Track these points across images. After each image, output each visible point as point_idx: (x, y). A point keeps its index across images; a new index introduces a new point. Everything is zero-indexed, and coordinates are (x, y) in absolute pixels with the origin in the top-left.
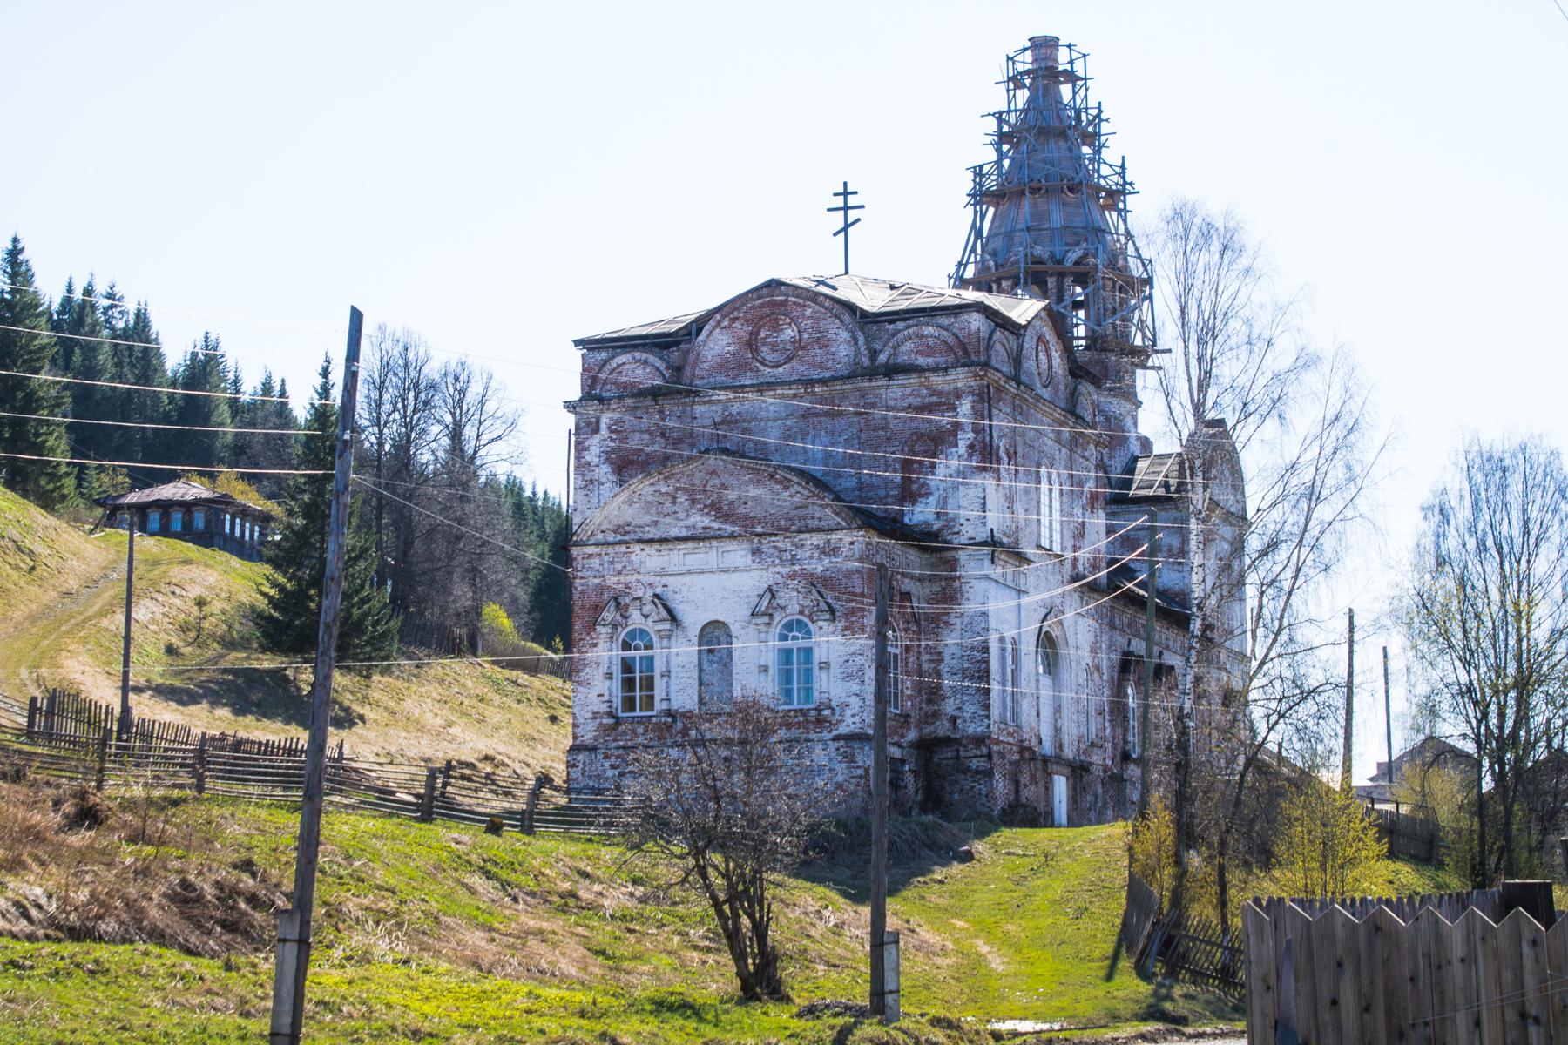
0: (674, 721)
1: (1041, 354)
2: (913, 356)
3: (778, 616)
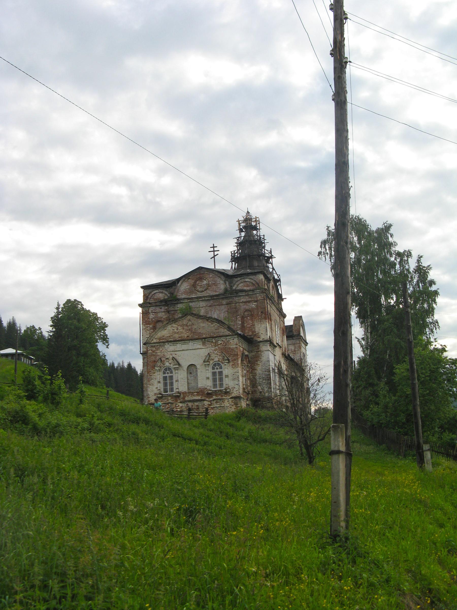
3: (211, 362)
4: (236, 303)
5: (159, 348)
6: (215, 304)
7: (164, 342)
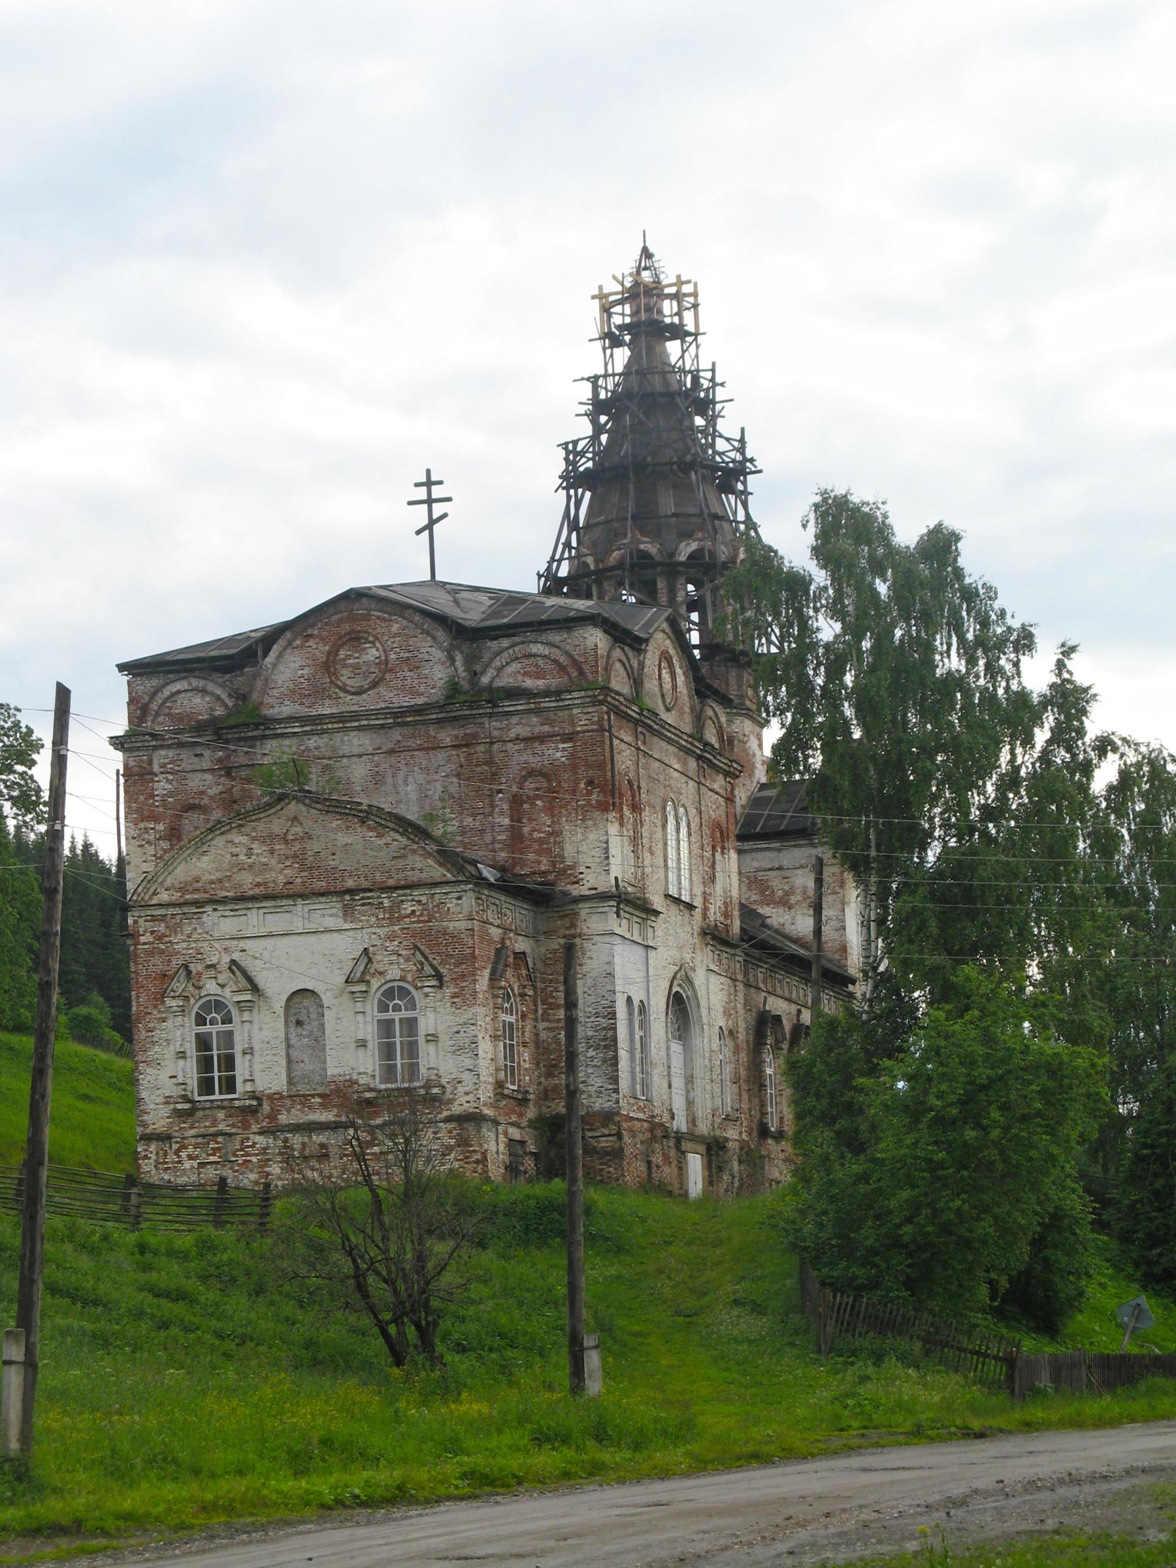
0: (260, 1105)
1: (664, 671)
2: (520, 678)
3: (375, 983)
4: (492, 743)
5: (179, 925)
6: (411, 743)
7: (198, 904)
